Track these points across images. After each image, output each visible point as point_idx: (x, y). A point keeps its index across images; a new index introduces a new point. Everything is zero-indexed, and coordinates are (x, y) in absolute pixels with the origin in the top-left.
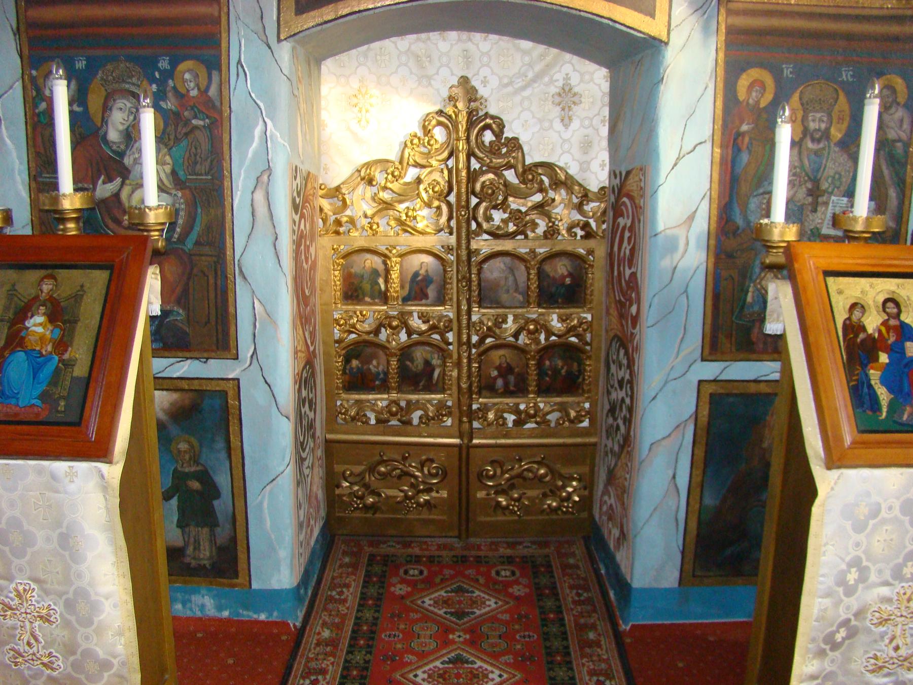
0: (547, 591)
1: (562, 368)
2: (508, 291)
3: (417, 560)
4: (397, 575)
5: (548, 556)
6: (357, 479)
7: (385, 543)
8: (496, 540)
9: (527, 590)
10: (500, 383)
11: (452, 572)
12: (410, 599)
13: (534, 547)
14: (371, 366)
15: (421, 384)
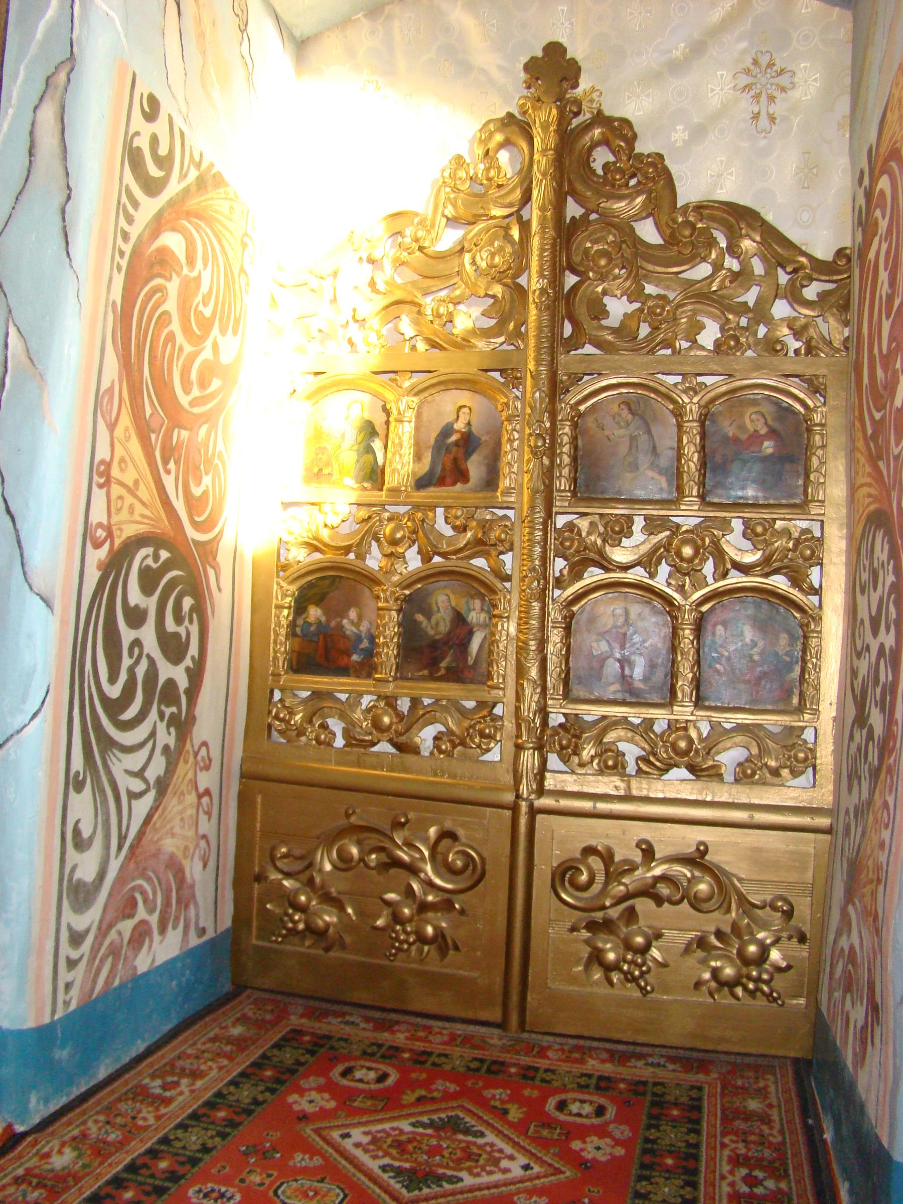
0: (669, 1161)
3: (392, 1053)
4: (324, 1072)
5: (700, 1089)
6: (298, 866)
7: (336, 1014)
9: (620, 1151)
11: (452, 1087)
12: (319, 1125)
13: (671, 1067)
14: (345, 621)
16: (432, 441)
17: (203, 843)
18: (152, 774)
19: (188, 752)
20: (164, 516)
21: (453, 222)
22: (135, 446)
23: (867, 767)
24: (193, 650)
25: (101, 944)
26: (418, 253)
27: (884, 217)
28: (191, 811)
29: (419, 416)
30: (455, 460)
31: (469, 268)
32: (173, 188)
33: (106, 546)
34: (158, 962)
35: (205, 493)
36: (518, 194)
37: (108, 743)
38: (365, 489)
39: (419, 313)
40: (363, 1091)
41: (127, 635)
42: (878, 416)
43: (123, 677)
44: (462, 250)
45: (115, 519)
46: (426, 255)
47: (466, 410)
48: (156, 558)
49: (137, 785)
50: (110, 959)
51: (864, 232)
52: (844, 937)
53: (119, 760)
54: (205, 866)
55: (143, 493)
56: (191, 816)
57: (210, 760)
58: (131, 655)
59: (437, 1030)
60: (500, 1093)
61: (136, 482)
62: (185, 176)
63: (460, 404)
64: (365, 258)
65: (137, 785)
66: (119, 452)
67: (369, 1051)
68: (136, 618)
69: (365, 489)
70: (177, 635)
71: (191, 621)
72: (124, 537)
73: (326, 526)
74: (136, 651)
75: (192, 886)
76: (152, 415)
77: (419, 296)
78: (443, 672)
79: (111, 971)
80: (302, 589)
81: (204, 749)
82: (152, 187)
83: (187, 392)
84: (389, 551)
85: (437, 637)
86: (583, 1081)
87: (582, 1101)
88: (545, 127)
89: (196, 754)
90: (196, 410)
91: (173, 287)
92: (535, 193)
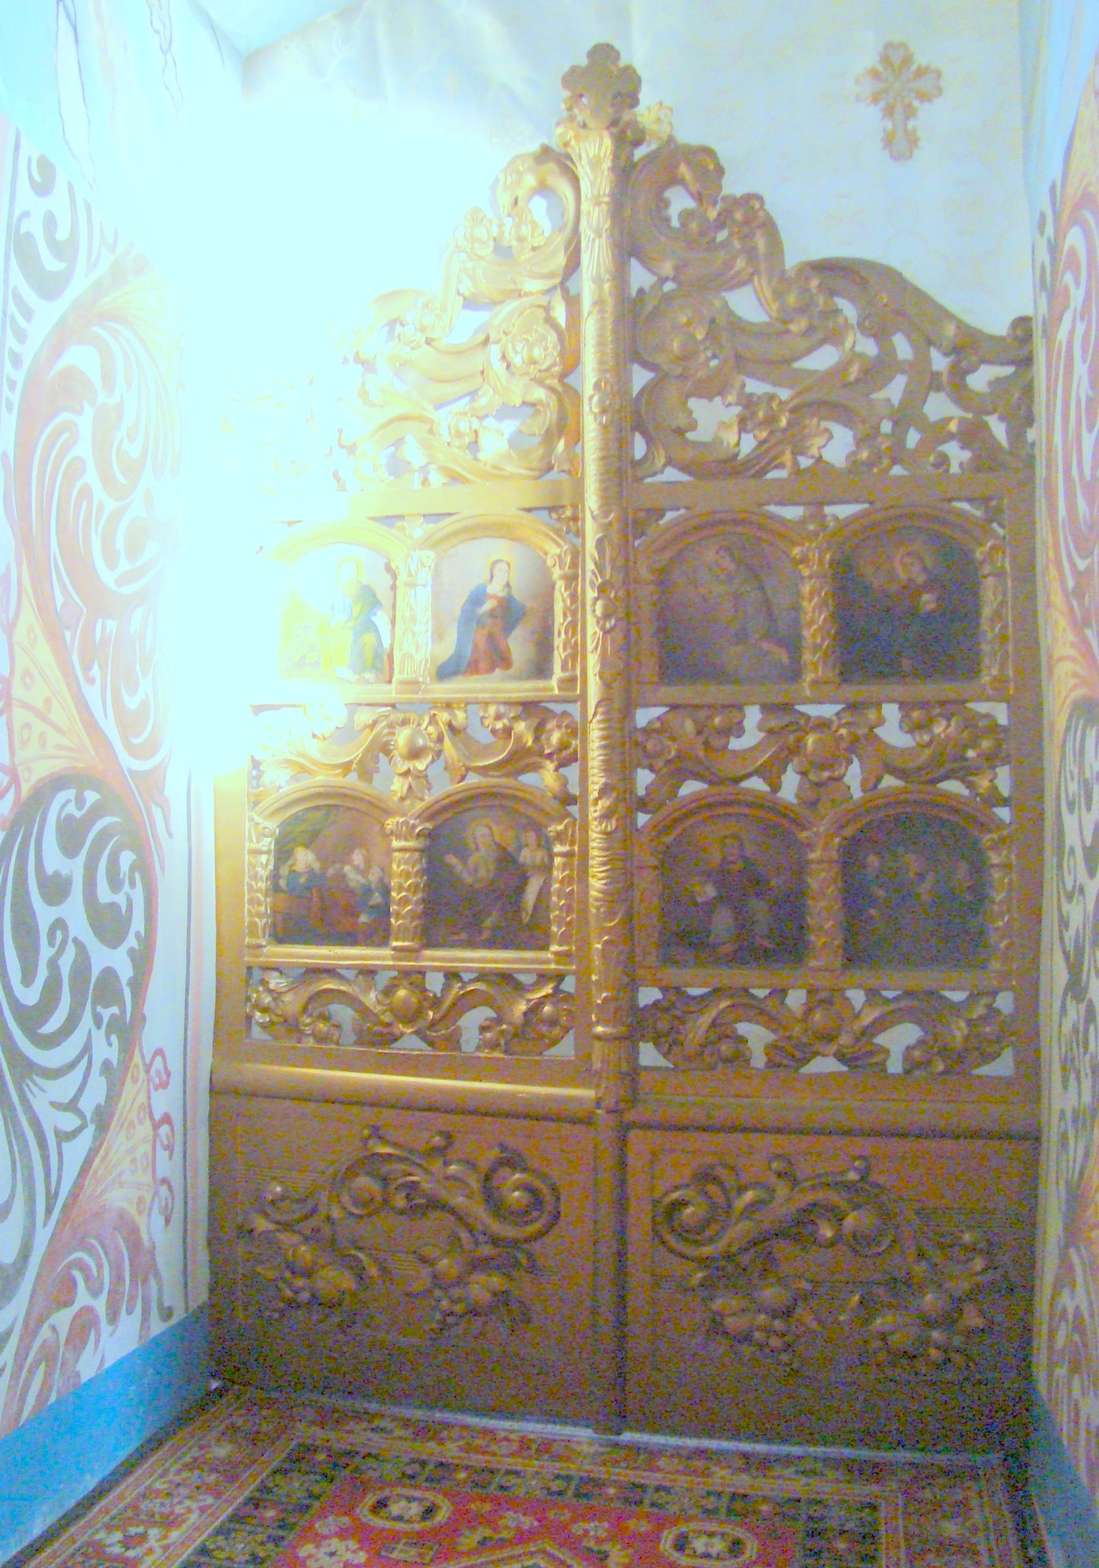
1: (921, 876)
2: (742, 636)
7: (358, 1417)
8: (761, 1448)
10: (722, 924)
11: (528, 1522)
13: (831, 1475)
14: (347, 869)
15: (488, 923)
16: (458, 612)
17: (164, 1189)
18: (87, 1105)
19: (137, 1066)
20: (88, 743)
21: (471, 303)
22: (44, 652)
23: (1087, 1057)
24: (138, 924)
25: (28, 1348)
26: (425, 347)
27: (1077, 283)
28: (145, 1148)
29: (437, 576)
30: (491, 637)
31: (499, 367)
32: (78, 286)
33: (11, 796)
34: (108, 1364)
35: (145, 703)
36: (561, 260)
37: (24, 1068)
38: (367, 682)
39: (431, 431)
40: (406, 1534)
41: (45, 915)
42: (1082, 565)
43: (43, 973)
44: (486, 341)
45: (21, 755)
46: (437, 350)
47: (502, 566)
48: (80, 801)
49: (69, 1122)
50: (42, 1367)
51: (1051, 298)
52: (1066, 1292)
53: (42, 1090)
54: (168, 1221)
55: (58, 715)
56: (145, 1154)
57: (168, 1074)
58: (51, 944)
59: (503, 1434)
60: (597, 1528)
61: (48, 701)
62: (96, 264)
63: (494, 558)
64: (351, 358)
65: (69, 1122)
66: (22, 661)
67: (409, 1472)
68: (56, 889)
69: (367, 682)
70: (114, 906)
71: (133, 884)
72: (34, 778)
73: (314, 736)
74: (59, 935)
75: (152, 1252)
76: (63, 605)
77: (430, 407)
78: (486, 935)
79: (44, 1383)
80: (283, 825)
81: (159, 1059)
82: (49, 287)
83: (112, 567)
84: (405, 768)
85: (477, 886)
86: (711, 1503)
87: (711, 1535)
88: (595, 164)
89: (148, 1068)
90: (126, 590)
91: (85, 422)
92: (585, 257)
